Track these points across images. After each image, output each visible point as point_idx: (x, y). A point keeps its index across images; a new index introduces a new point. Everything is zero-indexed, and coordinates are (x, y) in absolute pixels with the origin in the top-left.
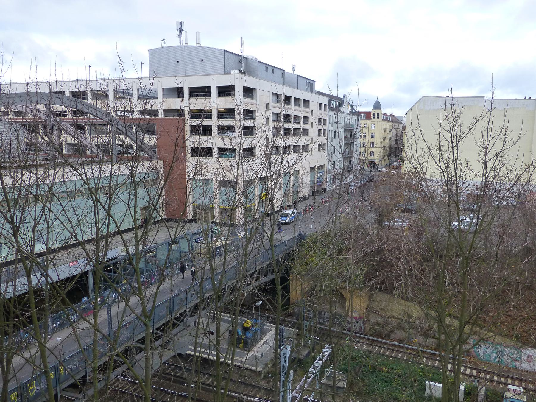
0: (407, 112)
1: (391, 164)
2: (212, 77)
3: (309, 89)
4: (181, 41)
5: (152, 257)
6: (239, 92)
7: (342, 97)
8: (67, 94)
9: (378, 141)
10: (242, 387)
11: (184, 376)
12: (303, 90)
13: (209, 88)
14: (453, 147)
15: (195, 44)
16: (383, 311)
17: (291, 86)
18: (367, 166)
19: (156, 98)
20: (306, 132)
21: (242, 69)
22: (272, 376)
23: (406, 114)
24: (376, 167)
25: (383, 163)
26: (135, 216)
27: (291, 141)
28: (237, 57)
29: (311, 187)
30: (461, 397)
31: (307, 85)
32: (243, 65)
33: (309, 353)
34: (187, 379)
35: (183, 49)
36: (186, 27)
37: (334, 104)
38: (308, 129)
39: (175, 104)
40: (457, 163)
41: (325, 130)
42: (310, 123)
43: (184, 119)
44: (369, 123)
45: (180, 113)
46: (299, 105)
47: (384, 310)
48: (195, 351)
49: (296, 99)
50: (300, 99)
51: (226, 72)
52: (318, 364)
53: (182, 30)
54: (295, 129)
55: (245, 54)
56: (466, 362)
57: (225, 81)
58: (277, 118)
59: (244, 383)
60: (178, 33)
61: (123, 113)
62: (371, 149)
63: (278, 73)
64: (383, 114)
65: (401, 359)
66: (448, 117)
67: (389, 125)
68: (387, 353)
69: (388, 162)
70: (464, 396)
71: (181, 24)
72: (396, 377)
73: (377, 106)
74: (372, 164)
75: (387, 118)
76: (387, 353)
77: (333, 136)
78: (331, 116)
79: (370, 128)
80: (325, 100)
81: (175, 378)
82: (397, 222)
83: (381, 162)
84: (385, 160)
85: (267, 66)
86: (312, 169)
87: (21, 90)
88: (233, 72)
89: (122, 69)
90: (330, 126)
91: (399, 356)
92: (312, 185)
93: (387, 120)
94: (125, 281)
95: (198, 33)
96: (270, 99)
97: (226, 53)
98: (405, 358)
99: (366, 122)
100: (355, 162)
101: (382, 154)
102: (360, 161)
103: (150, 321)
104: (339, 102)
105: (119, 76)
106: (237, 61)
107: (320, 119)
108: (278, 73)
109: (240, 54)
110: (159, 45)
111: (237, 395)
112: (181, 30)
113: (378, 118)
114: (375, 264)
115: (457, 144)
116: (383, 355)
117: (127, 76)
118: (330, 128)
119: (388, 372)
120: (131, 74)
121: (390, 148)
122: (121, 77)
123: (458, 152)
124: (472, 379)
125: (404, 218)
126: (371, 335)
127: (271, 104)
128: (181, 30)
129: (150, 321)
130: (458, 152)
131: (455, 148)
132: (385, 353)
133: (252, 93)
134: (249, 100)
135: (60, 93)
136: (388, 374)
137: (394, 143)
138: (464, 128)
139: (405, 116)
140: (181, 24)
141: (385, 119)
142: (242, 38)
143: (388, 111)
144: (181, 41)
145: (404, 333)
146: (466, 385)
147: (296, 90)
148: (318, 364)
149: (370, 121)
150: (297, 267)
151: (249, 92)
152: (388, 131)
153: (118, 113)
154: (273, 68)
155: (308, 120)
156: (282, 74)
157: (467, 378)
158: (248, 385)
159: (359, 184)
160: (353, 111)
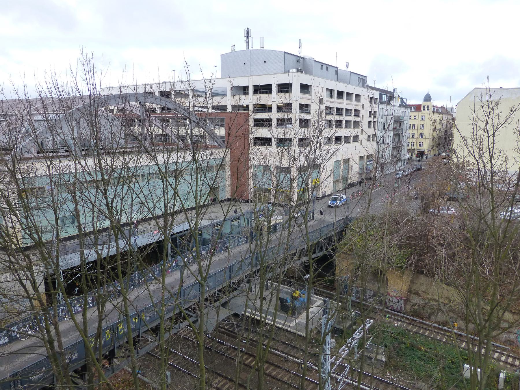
0: (458, 104)
1: (439, 154)
2: (273, 76)
3: (361, 84)
4: (248, 46)
5: (218, 230)
6: (296, 88)
7: (392, 91)
8: (157, 94)
9: (428, 132)
10: (288, 349)
11: (235, 331)
12: (355, 85)
13: (270, 86)
14: (488, 137)
15: (259, 48)
16: (424, 293)
17: (343, 81)
18: (415, 156)
19: (226, 95)
20: (357, 124)
21: (299, 68)
22: (315, 343)
23: (457, 106)
24: (425, 157)
25: (432, 154)
26: (196, 194)
27: (342, 132)
28: (295, 57)
29: (360, 174)
30: (501, 385)
31: (359, 81)
32: (301, 64)
33: (351, 326)
34: (237, 333)
35: (250, 53)
36: (252, 34)
37: (384, 98)
38: (358, 121)
39: (243, 100)
40: (492, 152)
41: (374, 122)
42: (361, 116)
43: (248, 113)
44: (419, 115)
45: (246, 108)
46: (351, 99)
47: (425, 292)
48: (261, 316)
49: (348, 94)
50: (352, 94)
51: (286, 71)
52: (357, 335)
53: (249, 36)
54: (346, 121)
55: (302, 55)
56: (509, 351)
57: (284, 79)
58: (330, 112)
59: (291, 345)
60: (245, 39)
61: (200, 109)
62: (421, 140)
63: (332, 71)
64: (433, 106)
65: (440, 341)
66: (484, 108)
67: (438, 117)
68: (427, 334)
69: (436, 152)
70: (504, 384)
71: (248, 31)
72: (434, 357)
73: (428, 98)
74: (421, 154)
75: (437, 110)
76: (427, 334)
77: (382, 128)
78: (381, 109)
79: (420, 119)
80: (377, 95)
81: (228, 332)
82: (443, 209)
83: (429, 152)
84: (434, 150)
85: (322, 64)
86: (361, 158)
87: (116, 92)
88: (291, 71)
89: (187, 71)
90: (380, 118)
91: (421, 331)
92: (361, 172)
93: (437, 112)
94: (195, 249)
95: (262, 38)
96: (325, 95)
97: (286, 54)
98: (444, 340)
99: (417, 114)
100: (404, 151)
101: (431, 144)
102: (409, 151)
103: (205, 282)
104: (390, 95)
105: (185, 79)
106: (296, 61)
107: (370, 112)
108: (332, 71)
109: (298, 54)
110: (229, 50)
111: (283, 355)
112: (248, 36)
113: (428, 110)
114: (418, 248)
115: (494, 134)
116: (422, 335)
117: (193, 78)
118: (380, 120)
119: (426, 351)
120: (196, 76)
121: (440, 138)
122: (186, 80)
123: (494, 142)
124: (514, 368)
125: (450, 206)
126: (412, 315)
127: (325, 99)
128: (248, 36)
129: (205, 282)
130: (494, 142)
131: (491, 138)
132: (424, 333)
133: (308, 89)
134: (305, 96)
135: (150, 93)
136: (426, 353)
137: (443, 134)
138: (502, 118)
139: (455, 107)
140: (248, 31)
141: (435, 111)
142: (300, 40)
143: (436, 103)
144: (248, 46)
145: (445, 316)
146: (507, 373)
147: (348, 86)
148: (357, 335)
149: (420, 113)
150: (342, 248)
151: (305, 88)
152: (438, 123)
153: (196, 109)
154: (328, 66)
155: (359, 113)
156: (336, 71)
157: (508, 366)
158: (293, 347)
159: (407, 173)
160: (403, 104)
